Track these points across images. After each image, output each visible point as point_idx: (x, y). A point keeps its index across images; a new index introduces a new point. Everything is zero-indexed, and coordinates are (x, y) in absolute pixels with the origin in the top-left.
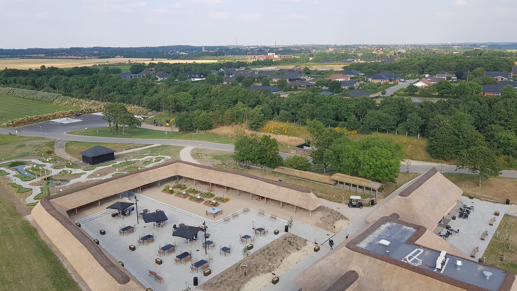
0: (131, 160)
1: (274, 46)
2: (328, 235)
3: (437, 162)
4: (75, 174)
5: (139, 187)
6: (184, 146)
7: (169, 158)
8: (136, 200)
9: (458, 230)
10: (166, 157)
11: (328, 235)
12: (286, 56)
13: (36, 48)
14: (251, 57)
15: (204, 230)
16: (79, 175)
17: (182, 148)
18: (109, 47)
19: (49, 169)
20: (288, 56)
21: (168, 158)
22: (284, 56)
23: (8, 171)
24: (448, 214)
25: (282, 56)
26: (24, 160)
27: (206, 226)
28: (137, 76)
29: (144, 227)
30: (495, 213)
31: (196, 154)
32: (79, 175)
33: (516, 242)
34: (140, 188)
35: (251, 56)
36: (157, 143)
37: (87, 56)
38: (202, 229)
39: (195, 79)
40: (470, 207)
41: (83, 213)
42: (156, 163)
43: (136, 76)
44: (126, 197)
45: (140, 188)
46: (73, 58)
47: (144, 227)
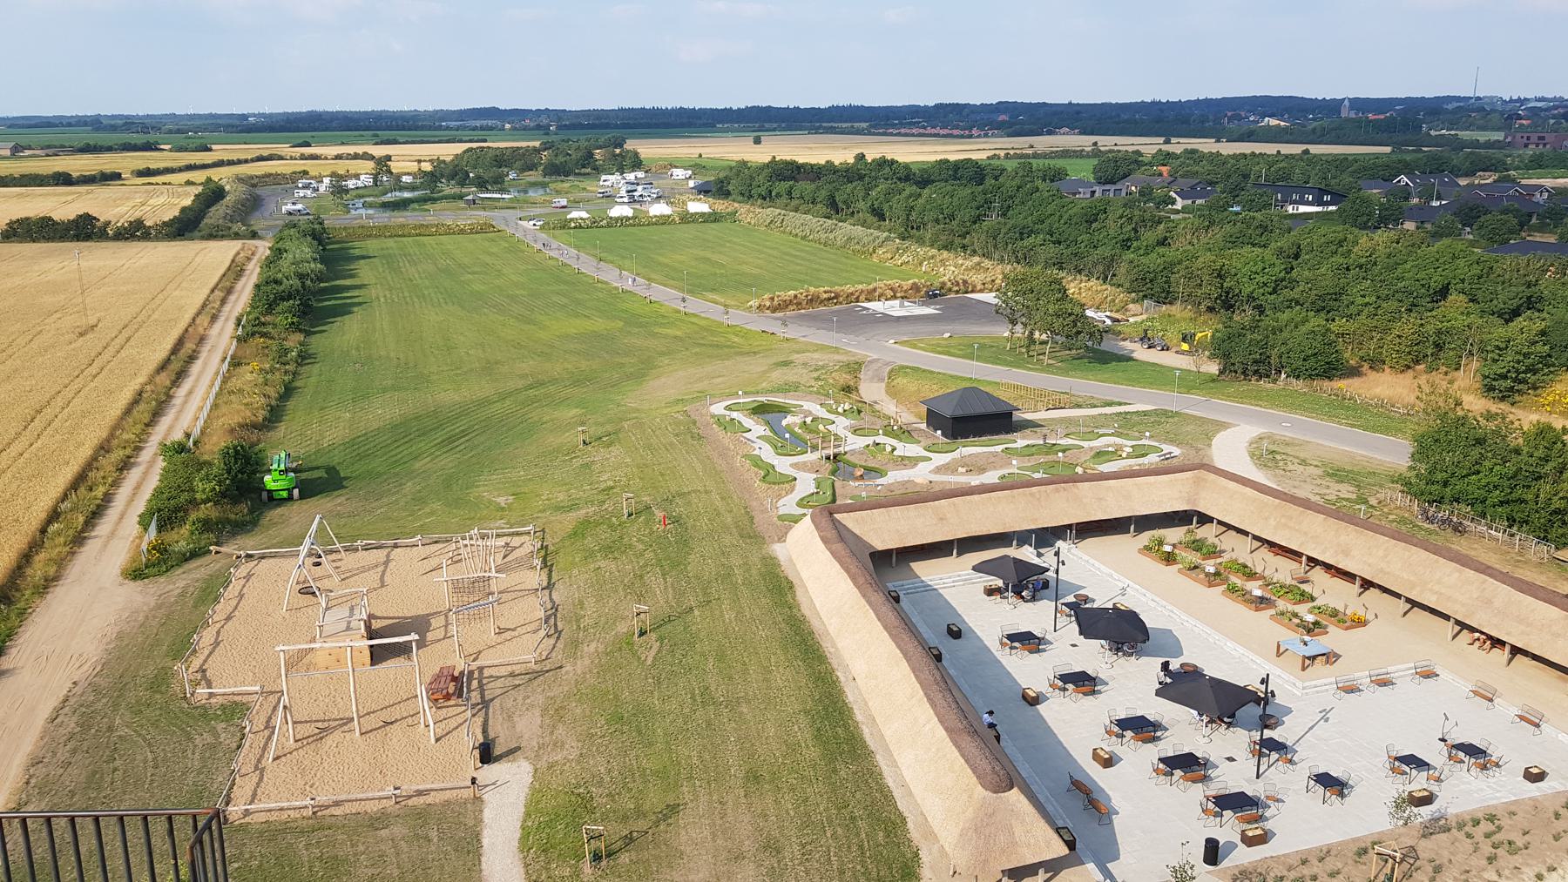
14: (1528, 138)
19: (842, 433)
27: (1269, 691)
35: (1528, 135)
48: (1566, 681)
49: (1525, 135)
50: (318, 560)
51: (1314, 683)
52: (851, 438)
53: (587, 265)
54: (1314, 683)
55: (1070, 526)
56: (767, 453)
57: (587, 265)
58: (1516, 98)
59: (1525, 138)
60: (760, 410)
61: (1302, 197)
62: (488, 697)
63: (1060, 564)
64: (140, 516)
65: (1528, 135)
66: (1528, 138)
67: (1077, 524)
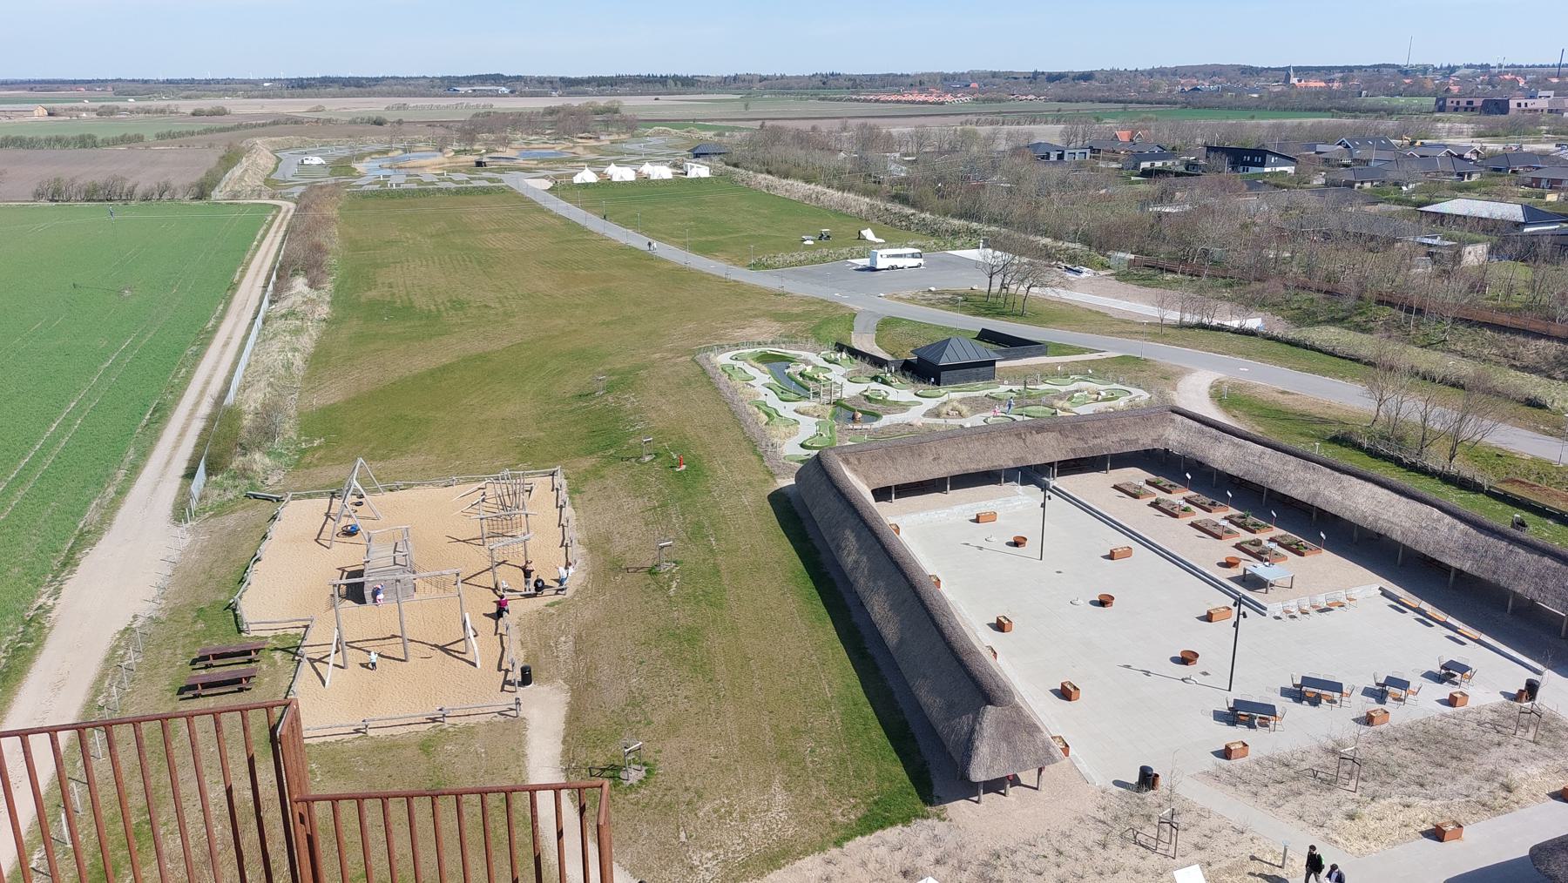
0: (1038, 387)
3: (297, 721)
4: (896, 403)
5: (1053, 463)
6: (1185, 366)
10: (1136, 392)
14: (1458, 103)
15: (506, 682)
16: (903, 407)
19: (840, 380)
21: (1140, 396)
23: (752, 372)
26: (788, 351)
27: (1241, 612)
28: (1077, 154)
29: (1058, 572)
33: (424, 882)
34: (1056, 465)
35: (1458, 99)
36: (1113, 349)
38: (510, 683)
42: (1107, 404)
43: (1074, 154)
45: (1056, 465)
47: (1058, 572)
48: (1567, 679)
49: (1455, 100)
50: (360, 500)
51: (576, 102)
52: (847, 385)
53: (594, 223)
54: (576, 102)
55: (1051, 464)
56: (773, 401)
57: (594, 223)
58: (1447, 65)
59: (1455, 102)
60: (765, 359)
61: (1252, 159)
62: (341, 572)
63: (1047, 499)
64: (1157, 776)
65: (1458, 99)
66: (1458, 103)
67: (1059, 462)
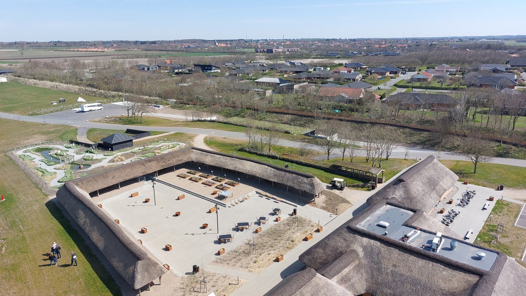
1: (282, 40)
2: (210, 230)
4: (96, 159)
7: (184, 144)
8: (153, 184)
9: (459, 212)
10: (181, 144)
11: (210, 230)
12: (293, 49)
13: (59, 41)
14: (261, 50)
16: (100, 161)
17: (197, 135)
18: (127, 40)
20: (295, 49)
21: (182, 145)
22: (291, 49)
23: (33, 156)
24: (444, 198)
25: (289, 49)
26: (49, 146)
30: (490, 198)
31: (207, 142)
32: (100, 161)
37: (106, 49)
39: (208, 71)
40: (473, 191)
41: (419, 221)
44: (144, 180)
46: (93, 51)
